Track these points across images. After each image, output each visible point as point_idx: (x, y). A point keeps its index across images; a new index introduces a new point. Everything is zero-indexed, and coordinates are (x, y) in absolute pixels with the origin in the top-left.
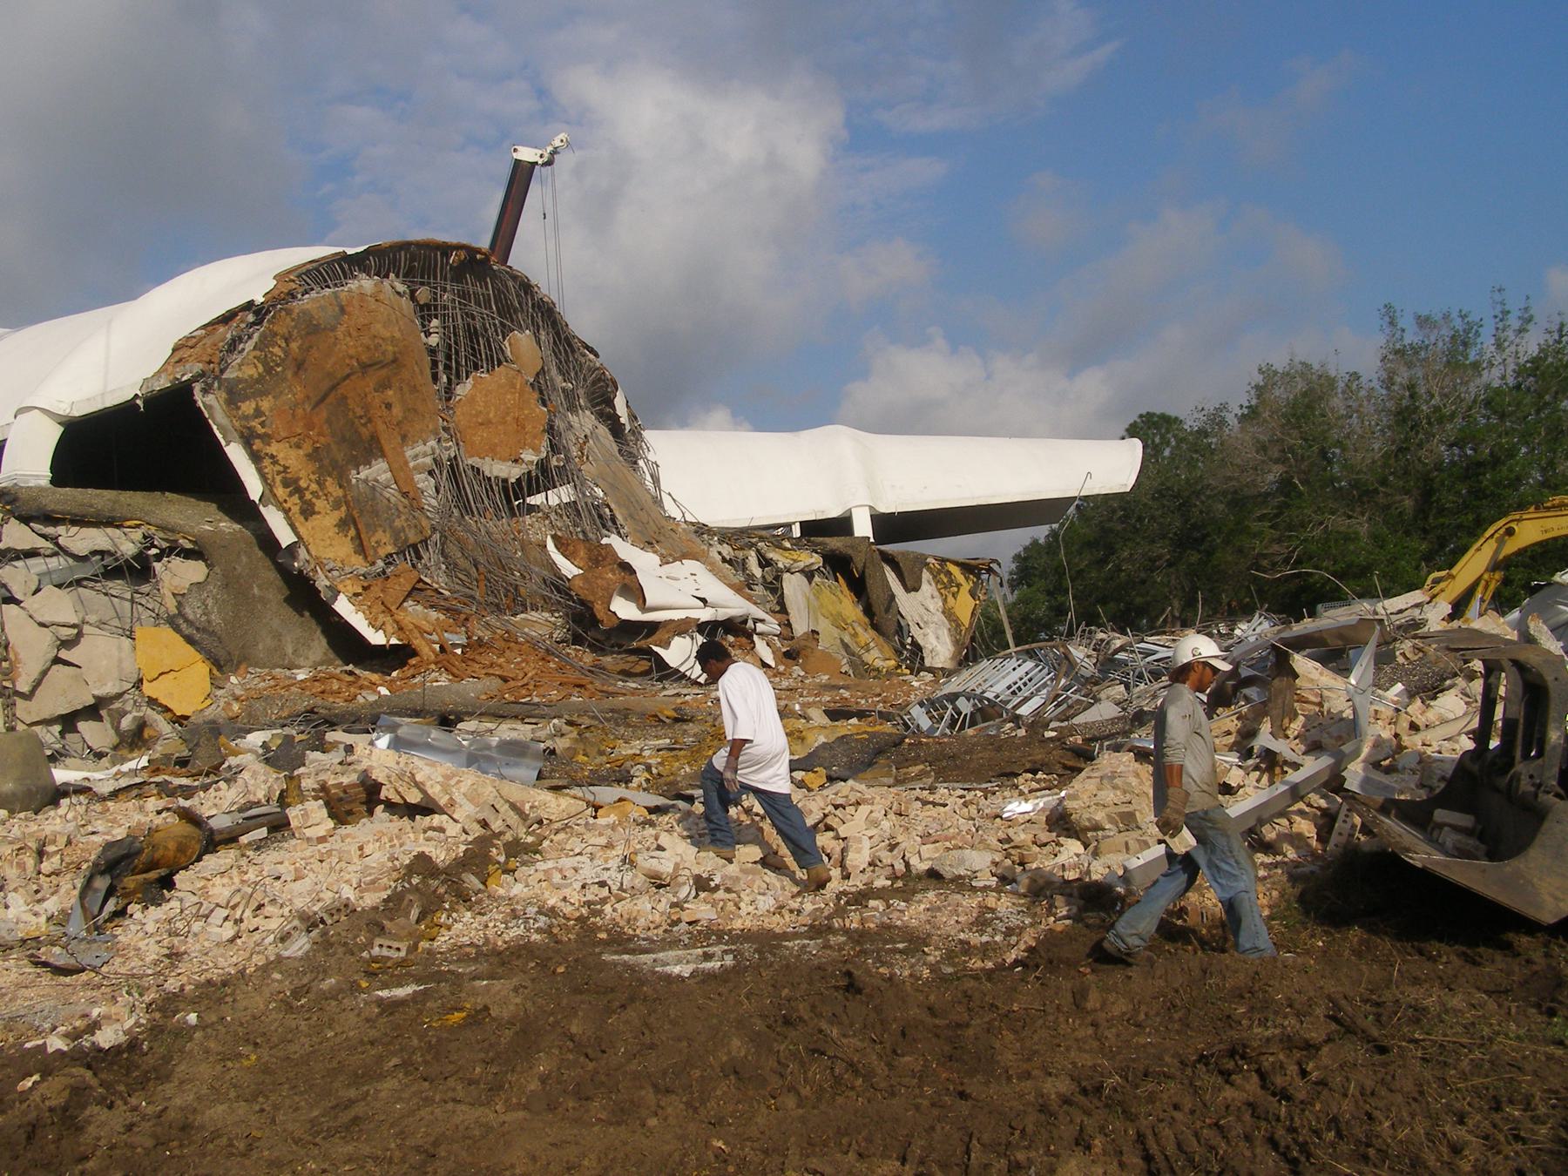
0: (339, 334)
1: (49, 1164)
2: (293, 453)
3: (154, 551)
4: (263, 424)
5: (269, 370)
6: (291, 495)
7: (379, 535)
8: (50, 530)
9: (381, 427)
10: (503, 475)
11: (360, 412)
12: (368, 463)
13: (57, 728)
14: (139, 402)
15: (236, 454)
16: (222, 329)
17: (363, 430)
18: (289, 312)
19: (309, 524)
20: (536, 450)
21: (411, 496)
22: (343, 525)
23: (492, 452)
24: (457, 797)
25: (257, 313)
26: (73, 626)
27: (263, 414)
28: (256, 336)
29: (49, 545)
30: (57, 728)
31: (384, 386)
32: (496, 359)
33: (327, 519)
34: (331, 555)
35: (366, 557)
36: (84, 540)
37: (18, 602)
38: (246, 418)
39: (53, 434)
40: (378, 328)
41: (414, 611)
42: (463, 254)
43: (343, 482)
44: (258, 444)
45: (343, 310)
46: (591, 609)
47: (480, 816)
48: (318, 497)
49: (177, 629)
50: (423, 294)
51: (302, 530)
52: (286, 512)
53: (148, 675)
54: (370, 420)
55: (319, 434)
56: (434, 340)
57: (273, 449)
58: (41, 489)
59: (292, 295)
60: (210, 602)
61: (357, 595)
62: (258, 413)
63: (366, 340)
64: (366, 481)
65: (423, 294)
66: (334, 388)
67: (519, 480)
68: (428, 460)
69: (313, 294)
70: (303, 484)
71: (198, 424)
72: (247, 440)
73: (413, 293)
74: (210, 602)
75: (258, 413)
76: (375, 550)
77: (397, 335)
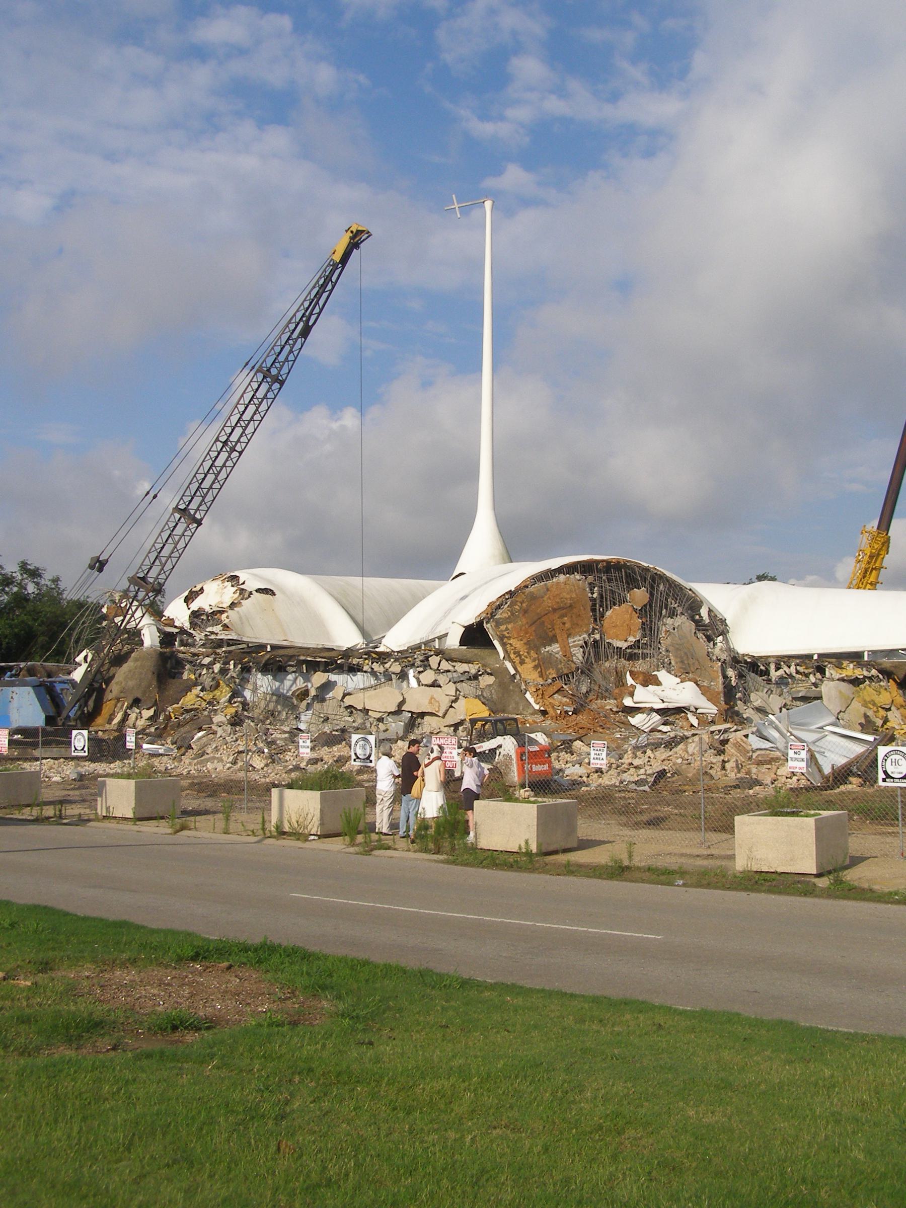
1: (649, 1124)
5: (512, 614)
8: (454, 664)
9: (558, 631)
11: (549, 626)
12: (550, 645)
13: (452, 728)
15: (496, 643)
20: (635, 637)
21: (568, 655)
22: (536, 667)
23: (617, 637)
30: (452, 728)
32: (623, 601)
33: (529, 665)
36: (462, 667)
38: (502, 631)
40: (565, 595)
43: (538, 651)
44: (505, 640)
50: (590, 578)
56: (595, 596)
57: (511, 641)
58: (454, 650)
62: (507, 629)
63: (558, 600)
68: (582, 643)
72: (501, 639)
75: (507, 629)
77: (574, 596)
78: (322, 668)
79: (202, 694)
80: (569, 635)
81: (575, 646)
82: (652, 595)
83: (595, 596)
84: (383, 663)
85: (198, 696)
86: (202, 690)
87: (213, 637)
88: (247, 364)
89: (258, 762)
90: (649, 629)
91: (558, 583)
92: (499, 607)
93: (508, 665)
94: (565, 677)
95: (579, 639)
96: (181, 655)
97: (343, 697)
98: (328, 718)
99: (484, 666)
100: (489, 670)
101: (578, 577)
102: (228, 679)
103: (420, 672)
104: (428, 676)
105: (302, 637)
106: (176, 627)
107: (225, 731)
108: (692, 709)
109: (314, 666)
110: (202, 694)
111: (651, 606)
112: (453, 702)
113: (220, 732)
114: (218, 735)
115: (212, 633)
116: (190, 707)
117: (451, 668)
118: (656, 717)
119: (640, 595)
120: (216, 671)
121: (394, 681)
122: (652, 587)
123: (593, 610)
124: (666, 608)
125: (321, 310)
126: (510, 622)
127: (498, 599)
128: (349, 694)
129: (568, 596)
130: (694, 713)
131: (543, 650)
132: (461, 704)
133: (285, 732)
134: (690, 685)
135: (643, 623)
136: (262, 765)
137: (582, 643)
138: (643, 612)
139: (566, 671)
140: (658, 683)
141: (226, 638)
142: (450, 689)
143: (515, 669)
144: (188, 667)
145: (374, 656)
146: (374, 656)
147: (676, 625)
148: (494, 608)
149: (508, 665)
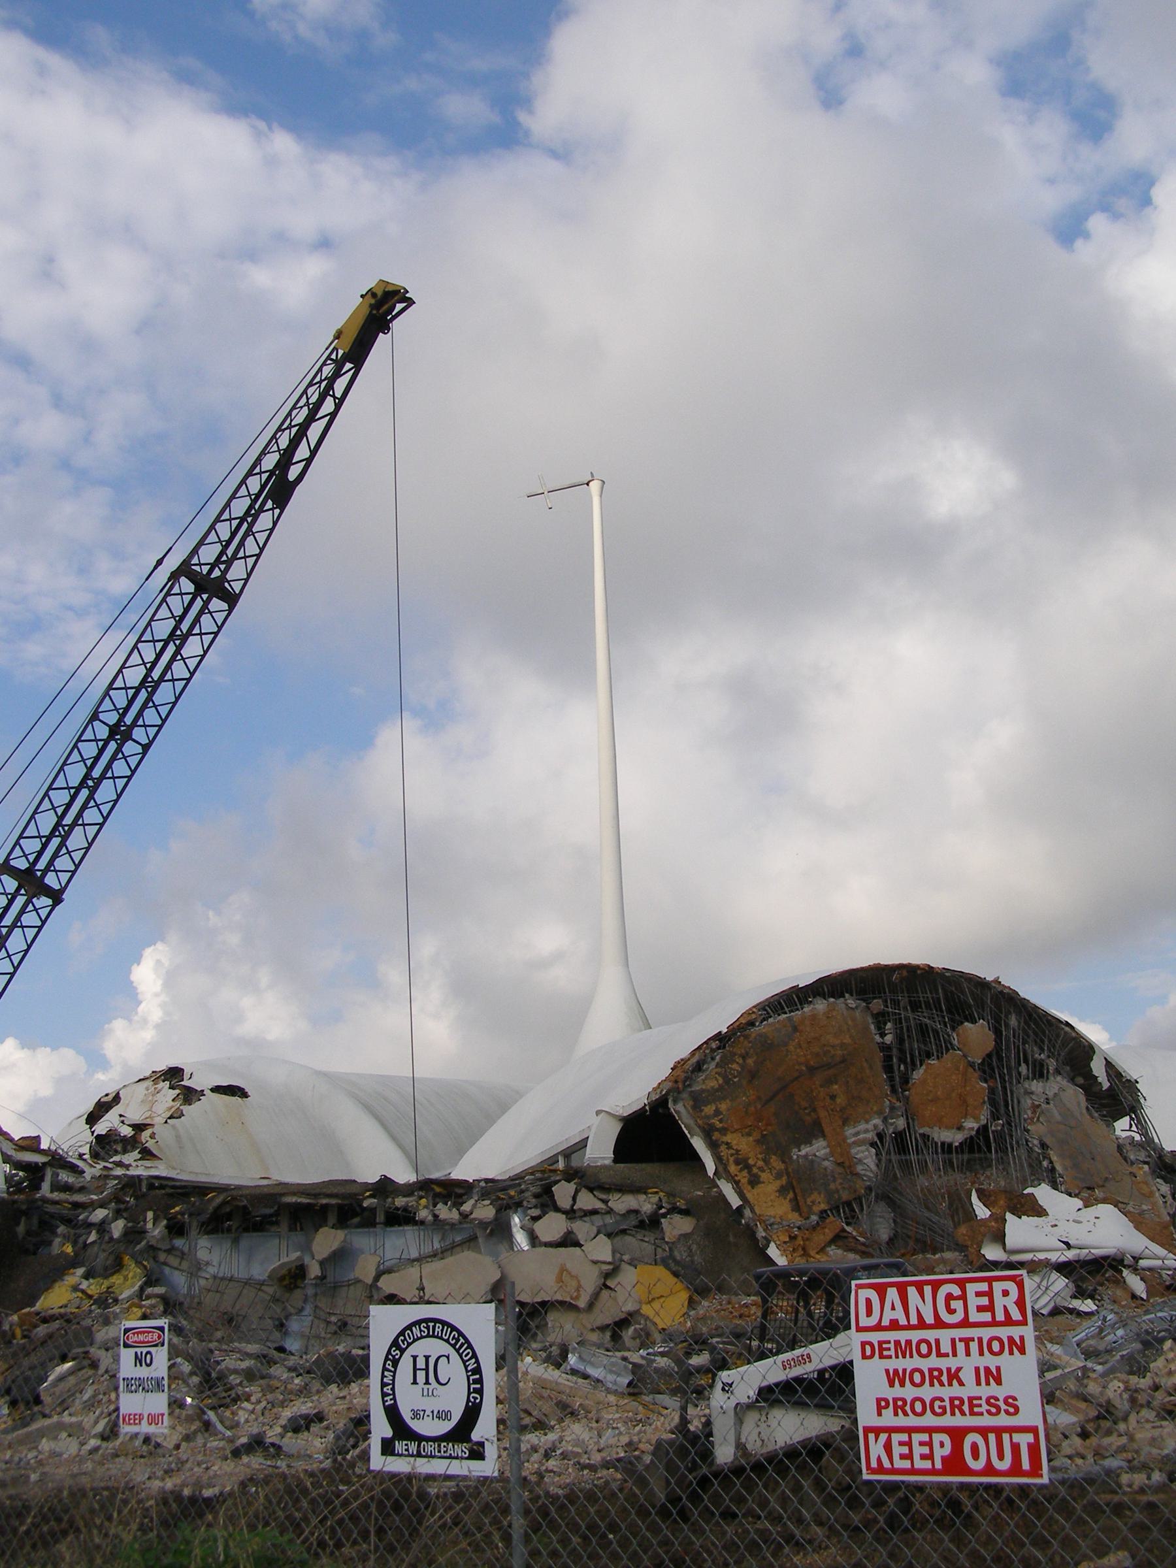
0: (791, 1048)
2: (744, 1140)
3: (663, 1211)
4: (721, 1121)
5: (727, 1081)
6: (741, 1170)
7: (815, 1196)
9: (822, 1114)
10: (948, 1140)
12: (809, 1142)
15: (698, 1144)
17: (808, 1118)
18: (746, 1037)
19: (755, 1191)
20: (977, 1119)
21: (847, 1166)
22: (782, 1191)
23: (940, 1122)
25: (720, 1040)
26: (609, 1263)
29: (602, 1206)
30: (608, 1334)
31: (829, 1082)
33: (770, 1186)
34: (772, 1213)
35: (800, 1215)
36: (621, 1203)
38: (708, 1117)
39: (615, 1129)
42: (905, 973)
43: (785, 1156)
46: (136, 1262)
48: (763, 1171)
49: (667, 1267)
50: (877, 1005)
51: (749, 1196)
52: (737, 1183)
54: (814, 1110)
55: (767, 1125)
56: (889, 1039)
57: (727, 1138)
58: (604, 1167)
59: (752, 1024)
60: (694, 1247)
62: (717, 1112)
64: (806, 1156)
67: (961, 1144)
68: (871, 1136)
69: (771, 1020)
70: (751, 1162)
71: (671, 1124)
74: (694, 1247)
75: (717, 1112)
76: (810, 1207)
77: (847, 1040)
78: (332, 1219)
79: (84, 1285)
80: (845, 1122)
82: (997, 1032)
83: (889, 1039)
84: (457, 1205)
85: (75, 1288)
86: (87, 1276)
87: (119, 1172)
88: (160, 562)
90: (1000, 1104)
91: (814, 1017)
92: (698, 1067)
93: (727, 1189)
94: (849, 1209)
95: (866, 1128)
96: (51, 1209)
97: (377, 1278)
98: (345, 1324)
99: (670, 1195)
100: (681, 1204)
101: (851, 1002)
102: (141, 1252)
103: (535, 1219)
104: (552, 1226)
105: (300, 1169)
108: (1128, 1260)
110: (84, 1285)
111: (1000, 1058)
112: (607, 1275)
114: (101, 1370)
115: (120, 1164)
117: (599, 1205)
118: (1059, 1283)
119: (976, 1036)
120: (116, 1235)
121: (480, 1240)
122: (997, 1020)
123: (888, 1069)
124: (1026, 1062)
125: (314, 453)
126: (724, 1098)
127: (693, 1053)
128: (389, 1271)
129: (837, 1042)
130: (1135, 1269)
131: (795, 1154)
132: (629, 1276)
133: (249, 1355)
134: (1106, 1211)
135: (992, 1091)
137: (871, 1136)
138: (990, 1066)
139: (845, 1196)
140: (1040, 1212)
141: (145, 1173)
142: (602, 1249)
143: (741, 1195)
144: (61, 1229)
145: (438, 1189)
146: (438, 1189)
147: (1050, 1094)
148: (687, 1073)
149: (727, 1189)
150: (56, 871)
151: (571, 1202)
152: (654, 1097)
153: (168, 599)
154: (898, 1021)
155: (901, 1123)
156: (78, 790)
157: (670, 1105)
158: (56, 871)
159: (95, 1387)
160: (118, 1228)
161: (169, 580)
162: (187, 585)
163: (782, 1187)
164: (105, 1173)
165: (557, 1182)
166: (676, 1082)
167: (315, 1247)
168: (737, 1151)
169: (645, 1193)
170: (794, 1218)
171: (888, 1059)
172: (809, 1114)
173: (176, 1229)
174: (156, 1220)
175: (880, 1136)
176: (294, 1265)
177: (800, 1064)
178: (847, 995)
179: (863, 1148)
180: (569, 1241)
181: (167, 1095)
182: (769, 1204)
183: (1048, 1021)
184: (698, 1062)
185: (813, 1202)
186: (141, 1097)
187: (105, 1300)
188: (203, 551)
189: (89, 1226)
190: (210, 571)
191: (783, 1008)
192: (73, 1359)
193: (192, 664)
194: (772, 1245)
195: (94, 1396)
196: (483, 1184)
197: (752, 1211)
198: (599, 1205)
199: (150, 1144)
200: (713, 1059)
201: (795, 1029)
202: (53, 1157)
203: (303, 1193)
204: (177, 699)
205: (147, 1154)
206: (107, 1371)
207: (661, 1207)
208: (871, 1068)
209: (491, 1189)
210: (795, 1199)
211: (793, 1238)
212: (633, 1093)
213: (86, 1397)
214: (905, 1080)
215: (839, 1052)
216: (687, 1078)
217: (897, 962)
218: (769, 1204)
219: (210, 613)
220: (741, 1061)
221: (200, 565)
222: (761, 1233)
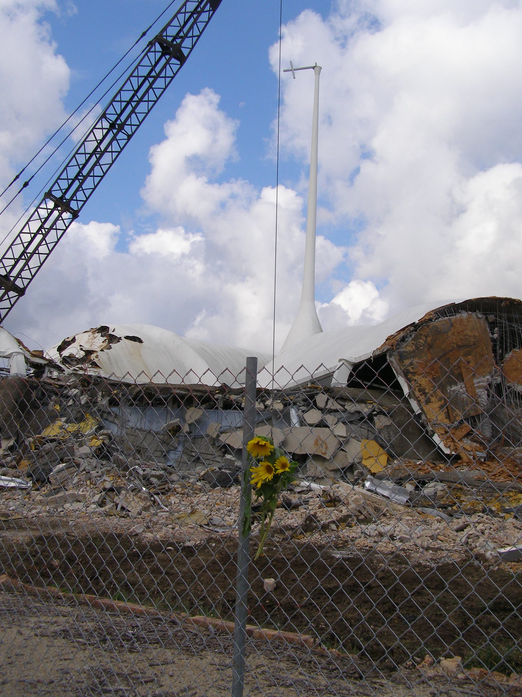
0: (449, 334)
3: (375, 413)
4: (413, 368)
5: (417, 348)
6: (421, 395)
9: (463, 370)
14: (372, 359)
15: (401, 380)
16: (402, 332)
18: (428, 326)
22: (441, 407)
24: (350, 501)
26: (345, 437)
27: (413, 364)
28: (413, 336)
29: (342, 408)
31: (466, 354)
33: (435, 404)
35: (450, 420)
36: (351, 407)
37: (329, 427)
40: (468, 332)
41: (467, 443)
45: (452, 325)
47: (358, 509)
48: (432, 396)
49: (377, 442)
53: (364, 458)
55: (436, 373)
56: (496, 336)
59: (430, 320)
60: (391, 433)
61: (442, 434)
62: (411, 364)
63: (462, 337)
64: (454, 391)
65: (491, 318)
66: (445, 355)
69: (440, 319)
70: (427, 391)
72: (406, 374)
73: (487, 318)
74: (391, 433)
76: (455, 417)
77: (476, 334)
81: (479, 387)
86: (66, 422)
87: (81, 372)
88: (144, 34)
89: (135, 505)
91: (461, 320)
92: (403, 339)
95: (482, 381)
104: (313, 416)
106: (44, 358)
107: (90, 464)
109: (190, 402)
113: (84, 464)
114: (81, 469)
116: (52, 438)
117: (339, 407)
123: (495, 351)
126: (414, 357)
129: (472, 334)
136: (139, 509)
139: (472, 413)
142: (341, 430)
143: (422, 409)
150: (21, 278)
151: (325, 405)
152: (377, 353)
153: (149, 54)
154: (501, 328)
155: (499, 380)
156: (73, 181)
157: (388, 357)
158: (21, 278)
159: (78, 477)
160: (84, 399)
161: (148, 46)
162: (158, 47)
163: (441, 405)
164: (75, 372)
165: (317, 394)
166: (392, 346)
167: (187, 417)
168: (420, 385)
169: (365, 403)
170: (447, 421)
171: (495, 346)
172: (456, 369)
173: (113, 403)
174: (103, 396)
175: (490, 385)
176: (175, 425)
177: (453, 343)
178: (477, 311)
179: (481, 390)
180: (322, 424)
181: (99, 341)
182: (434, 413)
183: (294, 390)
184: (403, 337)
185: (456, 415)
186: (87, 340)
187: (77, 435)
188: (169, 29)
189: (67, 397)
190: (173, 41)
191: (446, 314)
192: (66, 462)
193: (105, 168)
194: (436, 435)
195: (78, 482)
196: (275, 392)
197: (426, 416)
198: (339, 407)
199: (96, 360)
200: (411, 336)
201: (452, 325)
202: (50, 362)
203: (183, 389)
204: (96, 187)
205: (95, 365)
206: (84, 470)
207: (374, 411)
208: (487, 349)
209: (279, 394)
210: (448, 412)
211: (446, 432)
212: (364, 350)
213: (74, 482)
214: (502, 357)
215: (472, 340)
216: (398, 344)
217: (504, 297)
218: (434, 413)
219: (100, 165)
220: (424, 339)
221: (167, 36)
222: (430, 428)
